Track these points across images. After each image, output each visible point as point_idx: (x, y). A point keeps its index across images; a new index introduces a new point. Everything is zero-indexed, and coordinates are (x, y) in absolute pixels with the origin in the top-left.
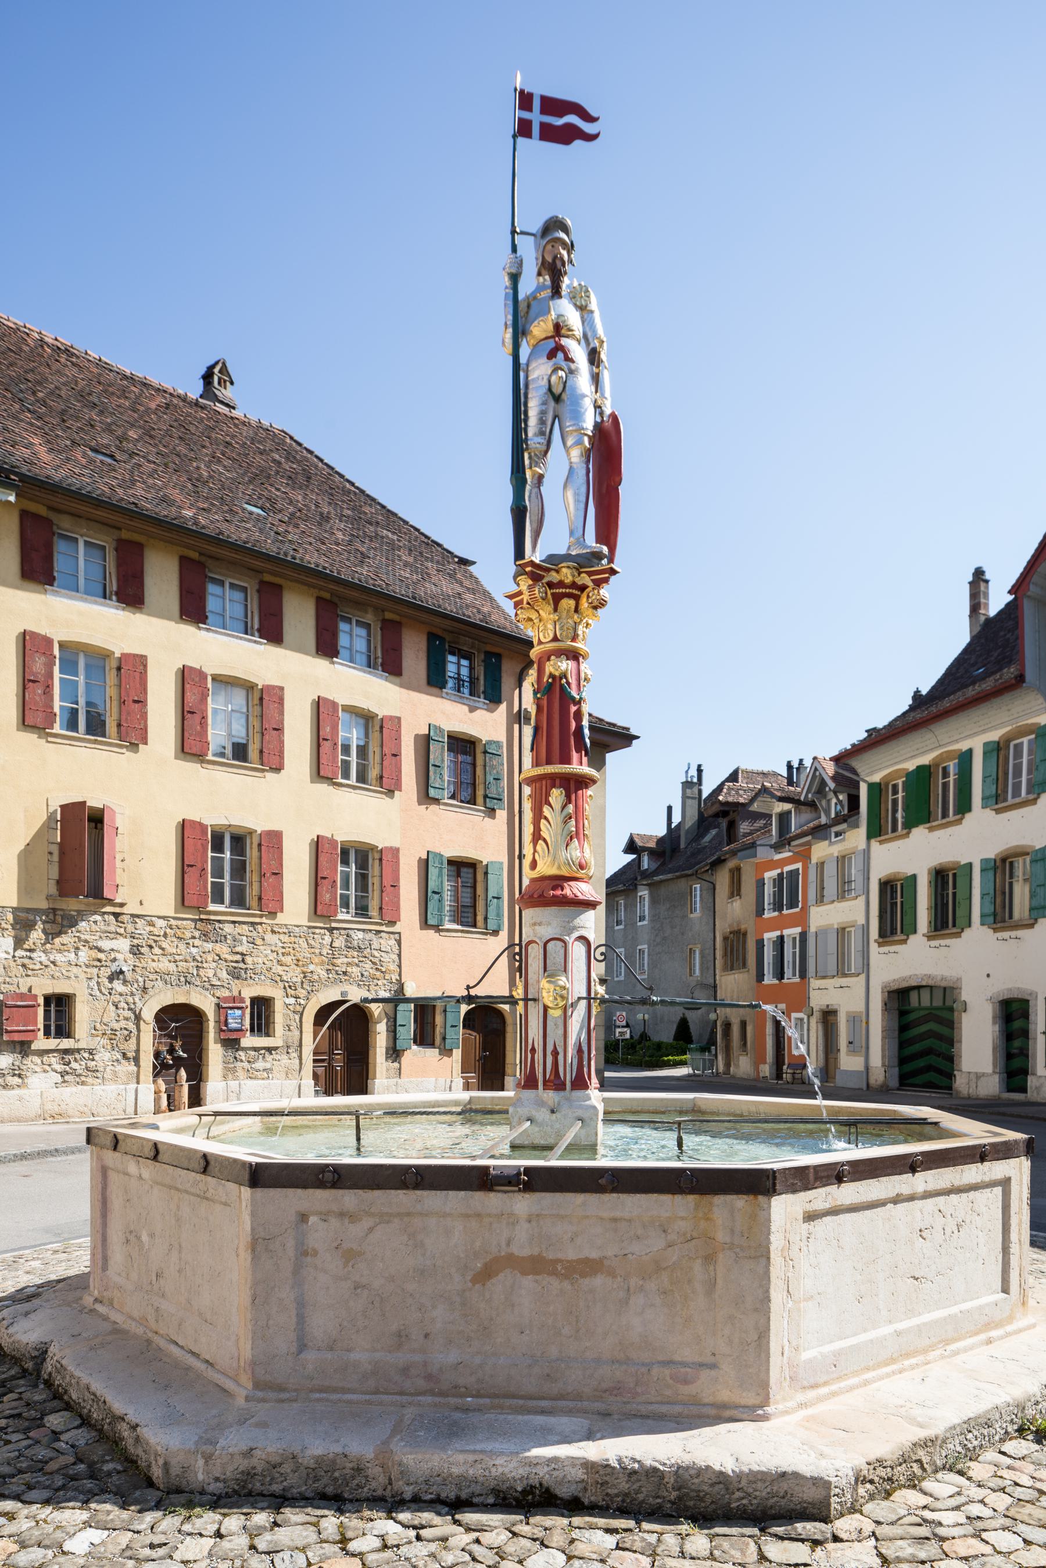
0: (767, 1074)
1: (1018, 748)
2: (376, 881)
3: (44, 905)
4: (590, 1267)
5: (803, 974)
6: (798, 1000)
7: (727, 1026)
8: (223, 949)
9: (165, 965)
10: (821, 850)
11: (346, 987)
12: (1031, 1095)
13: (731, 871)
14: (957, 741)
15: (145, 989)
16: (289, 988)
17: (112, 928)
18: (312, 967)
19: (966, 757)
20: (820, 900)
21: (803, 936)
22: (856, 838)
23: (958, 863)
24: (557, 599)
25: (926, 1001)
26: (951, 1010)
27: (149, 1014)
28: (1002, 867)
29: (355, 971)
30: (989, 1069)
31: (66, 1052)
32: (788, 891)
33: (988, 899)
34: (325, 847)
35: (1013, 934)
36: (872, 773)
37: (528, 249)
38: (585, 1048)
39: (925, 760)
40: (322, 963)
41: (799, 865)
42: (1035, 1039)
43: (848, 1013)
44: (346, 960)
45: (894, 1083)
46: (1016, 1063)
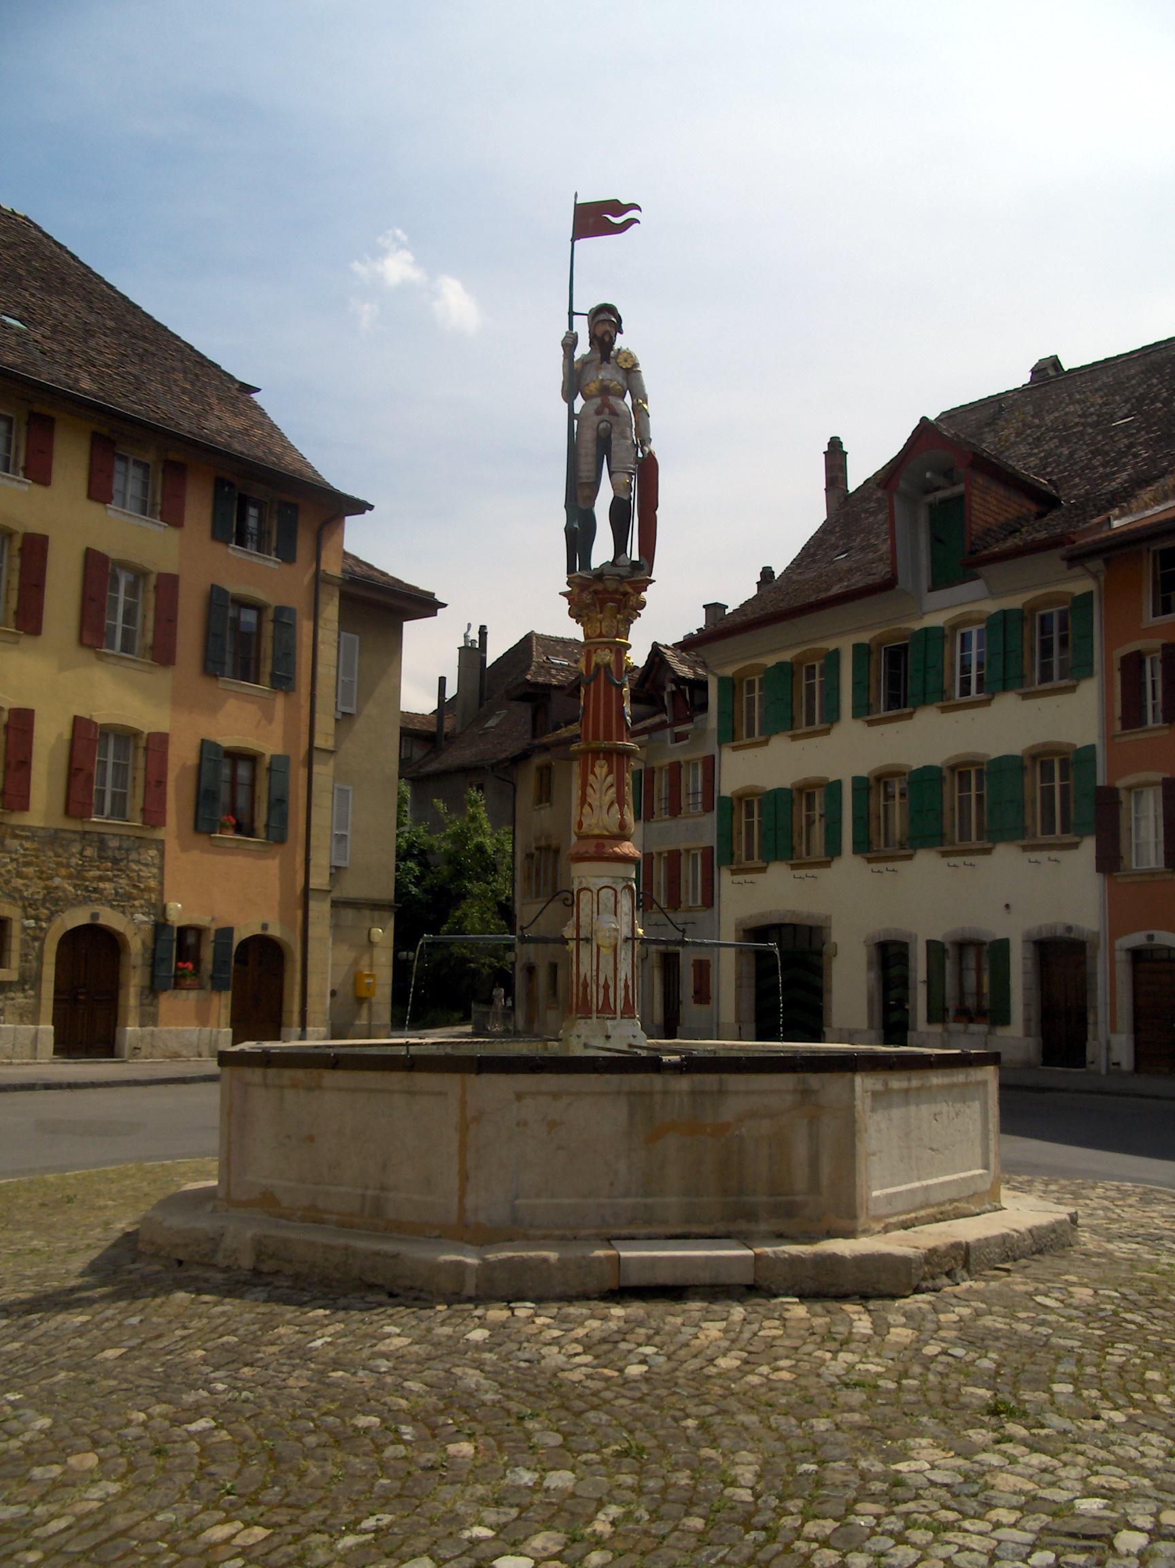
7: (530, 970)
11: (97, 908)
13: (539, 768)
14: (822, 639)
16: (29, 905)
18: (57, 881)
19: (835, 656)
23: (827, 779)
24: (602, 604)
26: (820, 954)
29: (107, 886)
30: (865, 1026)
35: (890, 865)
37: (582, 327)
38: (630, 983)
39: (787, 656)
40: (70, 877)
42: (916, 988)
44: (98, 873)
46: (895, 1017)
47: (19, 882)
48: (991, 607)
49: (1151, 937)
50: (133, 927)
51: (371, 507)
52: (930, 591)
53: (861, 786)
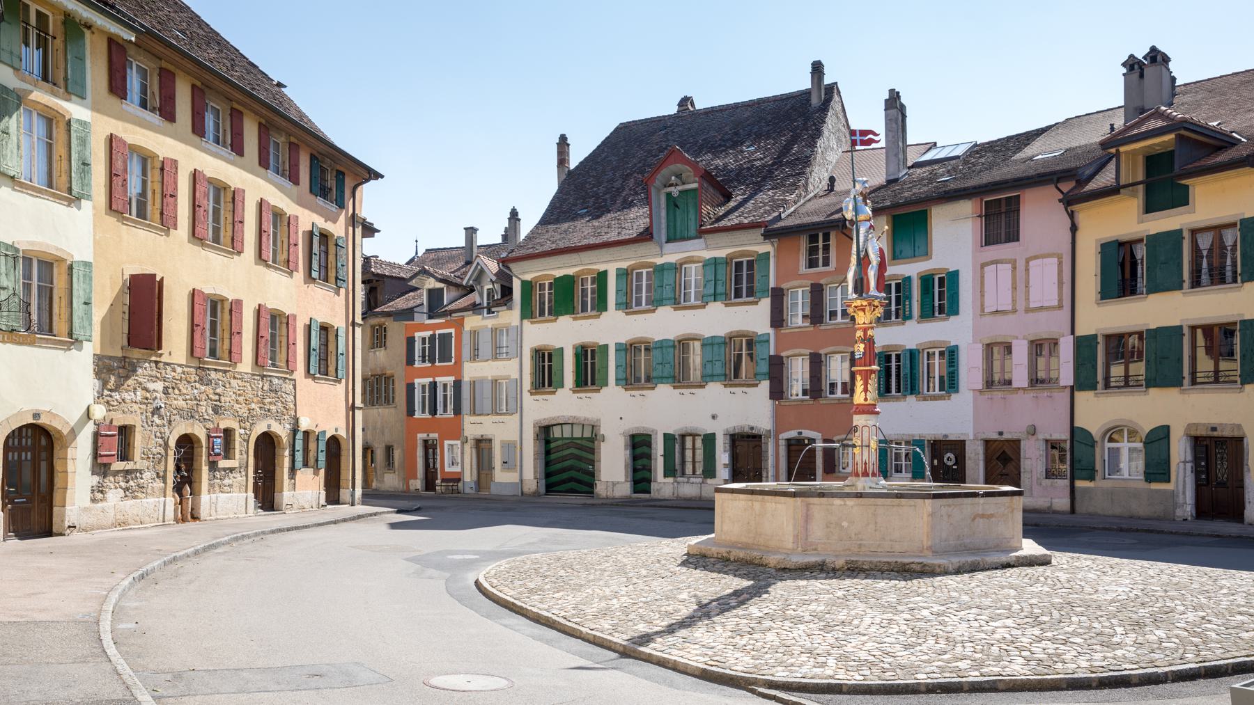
0: (419, 487)
1: (639, 275)
2: (284, 340)
3: (119, 354)
4: (992, 516)
5: (458, 410)
6: (455, 431)
8: (209, 390)
9: (180, 403)
10: (472, 322)
12: (654, 494)
15: (170, 422)
17: (154, 373)
18: (253, 406)
20: (475, 357)
21: (458, 385)
22: (510, 316)
25: (567, 434)
27: (172, 443)
28: (630, 349)
29: (273, 408)
30: (622, 479)
31: (127, 472)
32: (440, 349)
33: (621, 369)
34: (263, 313)
36: (524, 273)
41: (452, 330)
43: (502, 442)
45: (543, 490)
46: (640, 475)
47: (237, 407)
48: (708, 255)
49: (800, 433)
50: (281, 430)
51: (382, 177)
52: (667, 242)
53: (621, 348)
